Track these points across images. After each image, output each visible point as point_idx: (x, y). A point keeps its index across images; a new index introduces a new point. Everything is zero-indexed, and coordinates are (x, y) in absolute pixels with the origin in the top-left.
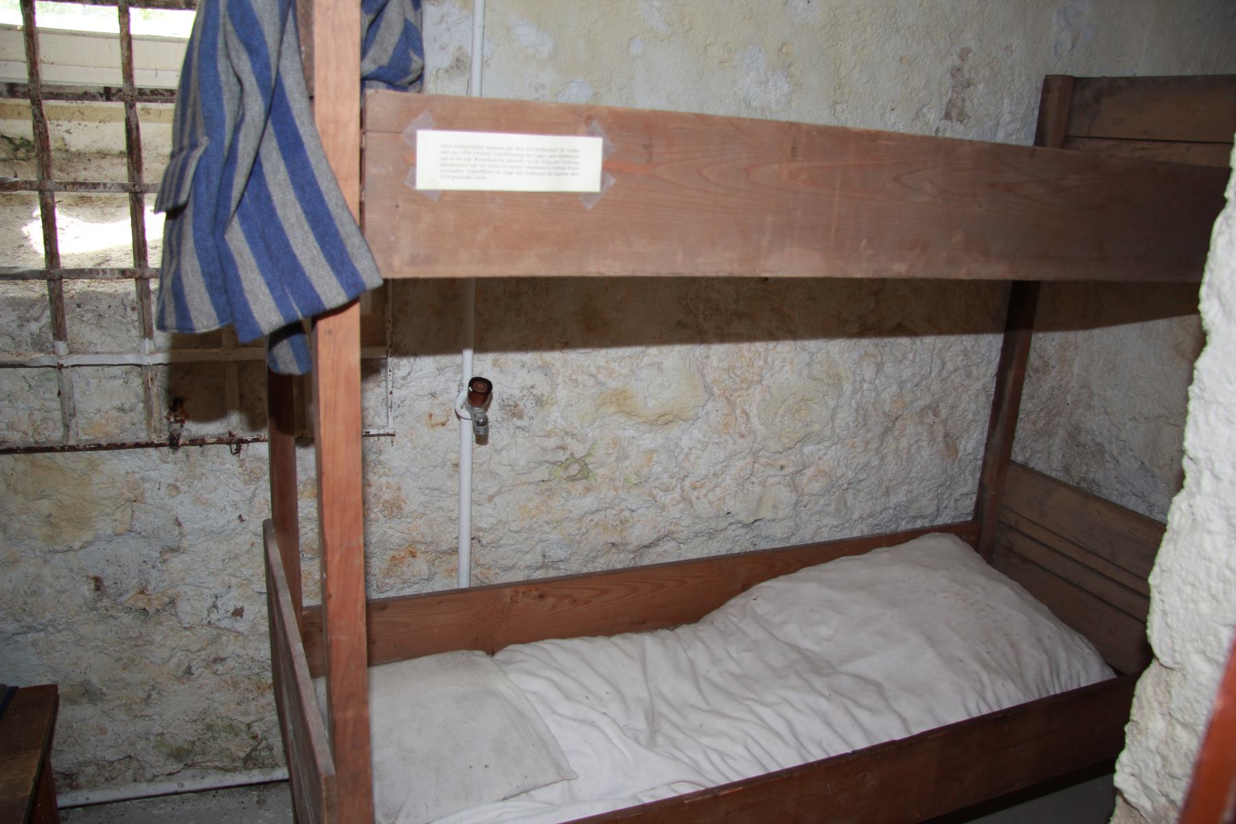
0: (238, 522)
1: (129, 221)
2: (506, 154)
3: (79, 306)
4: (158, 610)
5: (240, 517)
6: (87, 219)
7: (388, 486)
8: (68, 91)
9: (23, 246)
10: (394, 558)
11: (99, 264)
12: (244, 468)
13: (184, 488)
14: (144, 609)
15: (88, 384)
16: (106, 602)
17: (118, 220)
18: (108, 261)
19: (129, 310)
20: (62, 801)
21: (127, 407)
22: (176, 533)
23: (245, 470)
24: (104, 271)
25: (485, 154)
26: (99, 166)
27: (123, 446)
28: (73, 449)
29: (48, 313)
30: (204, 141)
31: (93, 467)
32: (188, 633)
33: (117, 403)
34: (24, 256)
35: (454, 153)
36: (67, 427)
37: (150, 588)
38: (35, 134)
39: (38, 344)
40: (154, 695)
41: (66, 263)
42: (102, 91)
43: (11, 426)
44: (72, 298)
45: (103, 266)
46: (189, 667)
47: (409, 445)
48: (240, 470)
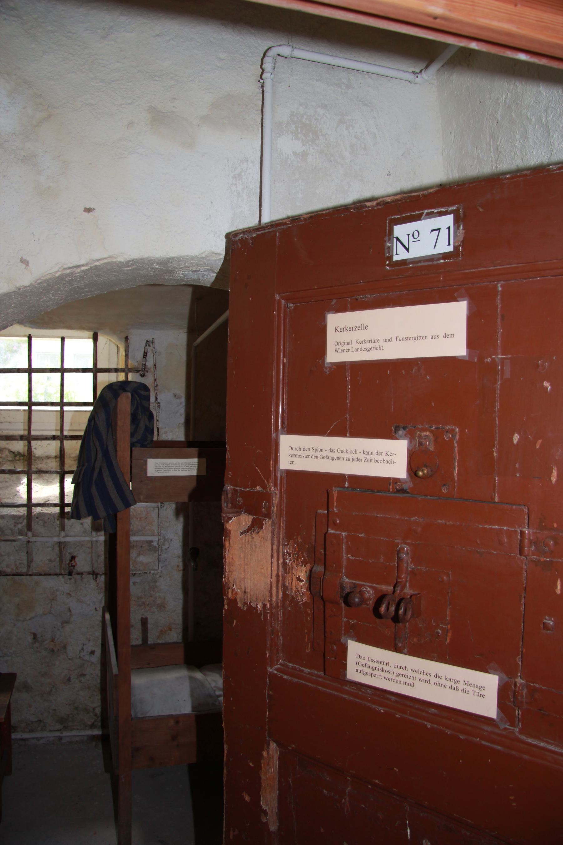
0: (95, 610)
1: (58, 484)
2: (175, 465)
3: (37, 518)
4: (58, 650)
5: (96, 609)
6: (41, 484)
7: (160, 597)
8: (40, 437)
9: (16, 495)
10: (161, 631)
11: (45, 502)
12: (98, 587)
13: (73, 594)
14: (53, 649)
15: (38, 550)
16: (37, 645)
17: (53, 485)
18: (49, 501)
19: (56, 520)
20: (13, 736)
21: (53, 559)
22: (69, 614)
23: (99, 588)
24: (48, 504)
25: (168, 465)
26: (46, 462)
27: (50, 575)
28: (30, 575)
29: (25, 521)
30: (86, 464)
31: (37, 583)
32: (70, 661)
33: (49, 558)
34: (17, 499)
35: (159, 465)
36: (29, 566)
37: (56, 639)
38: (27, 453)
39: (21, 533)
40: (54, 690)
41: (34, 501)
42: (52, 437)
43: (8, 566)
44: (35, 515)
45: (48, 502)
46: (70, 678)
47: (169, 579)
48: (97, 588)
